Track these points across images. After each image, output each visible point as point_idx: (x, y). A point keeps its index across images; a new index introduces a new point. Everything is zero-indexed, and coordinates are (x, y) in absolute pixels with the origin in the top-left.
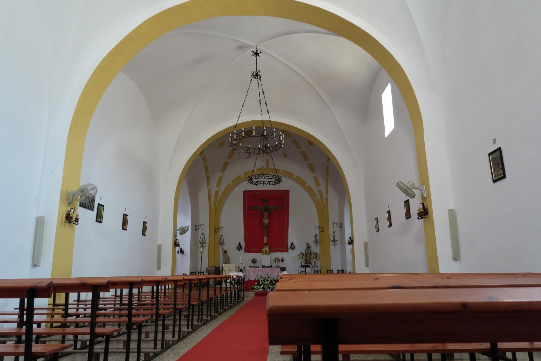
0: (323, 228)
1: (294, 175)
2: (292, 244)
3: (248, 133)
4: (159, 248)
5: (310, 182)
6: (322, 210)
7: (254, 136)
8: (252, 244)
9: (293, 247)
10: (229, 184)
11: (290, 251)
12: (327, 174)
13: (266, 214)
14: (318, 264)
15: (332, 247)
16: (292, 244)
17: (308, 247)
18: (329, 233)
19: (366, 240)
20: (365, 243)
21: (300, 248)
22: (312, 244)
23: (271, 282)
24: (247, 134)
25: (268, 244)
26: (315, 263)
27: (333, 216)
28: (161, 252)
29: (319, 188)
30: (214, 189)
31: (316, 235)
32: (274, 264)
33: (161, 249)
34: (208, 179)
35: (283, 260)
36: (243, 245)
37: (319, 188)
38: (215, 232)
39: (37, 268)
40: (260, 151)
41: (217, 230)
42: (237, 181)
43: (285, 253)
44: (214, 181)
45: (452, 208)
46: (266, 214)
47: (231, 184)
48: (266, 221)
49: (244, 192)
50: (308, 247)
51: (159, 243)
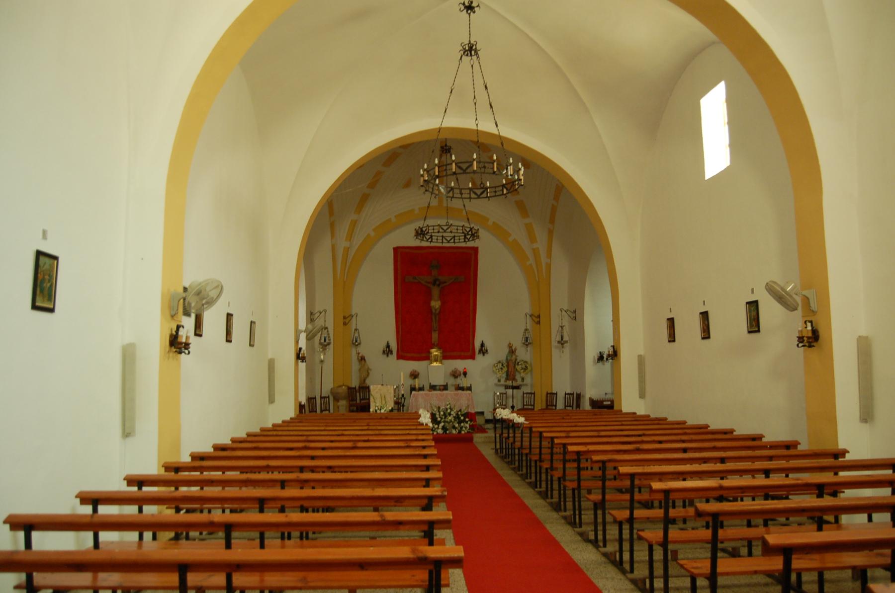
0: (539, 317)
1: (488, 220)
2: (482, 345)
3: (464, 166)
4: (271, 364)
5: (518, 234)
6: (539, 285)
7: (474, 172)
8: (411, 343)
9: (483, 351)
10: (369, 235)
11: (479, 357)
12: (552, 221)
13: (436, 292)
14: (528, 380)
15: (555, 353)
16: (482, 345)
17: (512, 351)
18: (550, 326)
19: (642, 353)
20: (640, 357)
21: (497, 353)
22: (517, 343)
23: (457, 417)
24: (460, 168)
25: (440, 346)
26: (523, 379)
27: (559, 300)
28: (274, 371)
29: (535, 246)
30: (342, 244)
31: (526, 330)
32: (451, 381)
33: (274, 368)
34: (332, 225)
35: (465, 374)
36: (394, 346)
37: (535, 246)
38: (345, 324)
39: (129, 440)
40: (473, 195)
41: (347, 320)
42: (385, 228)
43: (469, 361)
44: (343, 230)
45: (863, 333)
46: (436, 292)
47: (373, 234)
48: (436, 304)
49: (396, 250)
50: (512, 351)
51: (270, 357)
